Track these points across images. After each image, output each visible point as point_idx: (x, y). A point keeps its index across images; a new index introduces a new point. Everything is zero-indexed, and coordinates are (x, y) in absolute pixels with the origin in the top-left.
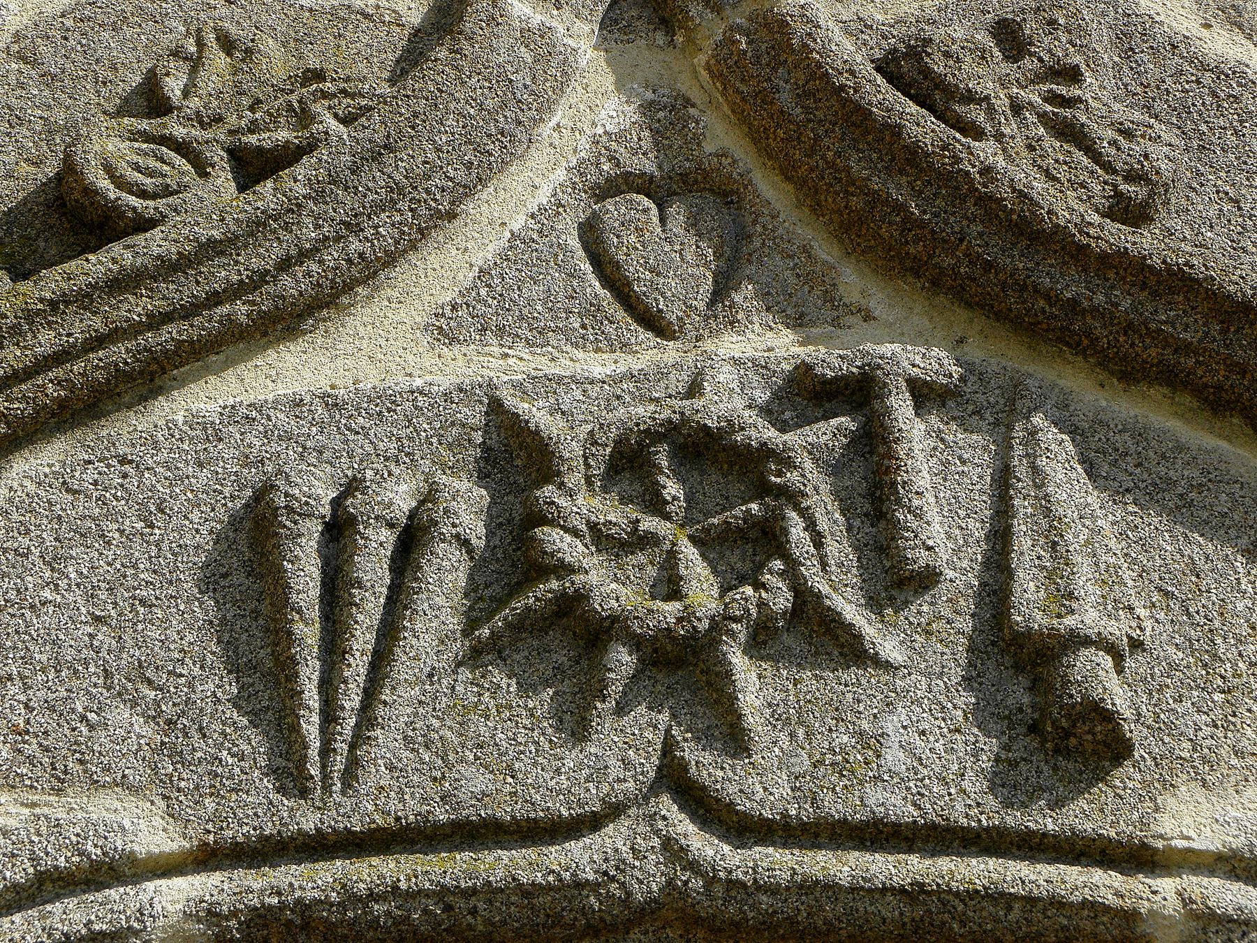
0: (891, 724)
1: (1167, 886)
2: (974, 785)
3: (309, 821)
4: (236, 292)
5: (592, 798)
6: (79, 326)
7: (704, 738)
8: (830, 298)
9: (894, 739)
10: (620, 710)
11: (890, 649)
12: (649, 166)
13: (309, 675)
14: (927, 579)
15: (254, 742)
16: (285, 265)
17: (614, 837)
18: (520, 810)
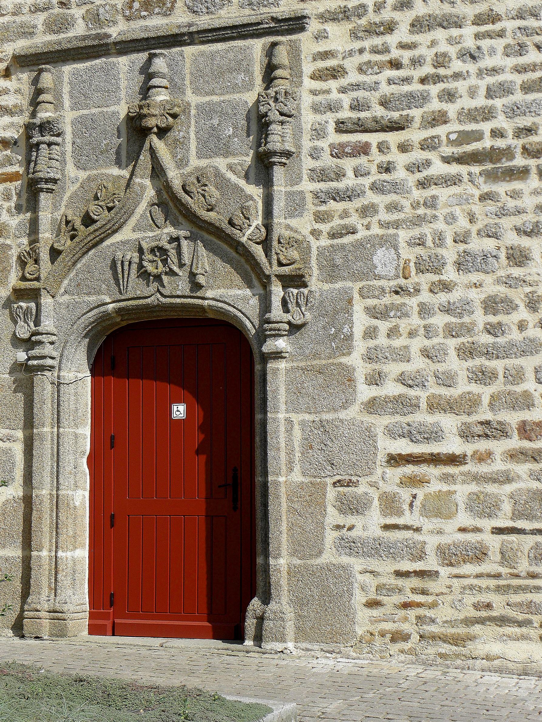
0: (180, 283)
1: (207, 301)
2: (188, 290)
3: (123, 298)
4: (109, 229)
5: (150, 294)
6: (92, 236)
7: (161, 286)
8: (178, 222)
9: (180, 285)
10: (152, 283)
11: (181, 274)
12: (157, 202)
13: (121, 283)
14: (185, 265)
15: (117, 288)
17: (152, 298)
18: (143, 296)
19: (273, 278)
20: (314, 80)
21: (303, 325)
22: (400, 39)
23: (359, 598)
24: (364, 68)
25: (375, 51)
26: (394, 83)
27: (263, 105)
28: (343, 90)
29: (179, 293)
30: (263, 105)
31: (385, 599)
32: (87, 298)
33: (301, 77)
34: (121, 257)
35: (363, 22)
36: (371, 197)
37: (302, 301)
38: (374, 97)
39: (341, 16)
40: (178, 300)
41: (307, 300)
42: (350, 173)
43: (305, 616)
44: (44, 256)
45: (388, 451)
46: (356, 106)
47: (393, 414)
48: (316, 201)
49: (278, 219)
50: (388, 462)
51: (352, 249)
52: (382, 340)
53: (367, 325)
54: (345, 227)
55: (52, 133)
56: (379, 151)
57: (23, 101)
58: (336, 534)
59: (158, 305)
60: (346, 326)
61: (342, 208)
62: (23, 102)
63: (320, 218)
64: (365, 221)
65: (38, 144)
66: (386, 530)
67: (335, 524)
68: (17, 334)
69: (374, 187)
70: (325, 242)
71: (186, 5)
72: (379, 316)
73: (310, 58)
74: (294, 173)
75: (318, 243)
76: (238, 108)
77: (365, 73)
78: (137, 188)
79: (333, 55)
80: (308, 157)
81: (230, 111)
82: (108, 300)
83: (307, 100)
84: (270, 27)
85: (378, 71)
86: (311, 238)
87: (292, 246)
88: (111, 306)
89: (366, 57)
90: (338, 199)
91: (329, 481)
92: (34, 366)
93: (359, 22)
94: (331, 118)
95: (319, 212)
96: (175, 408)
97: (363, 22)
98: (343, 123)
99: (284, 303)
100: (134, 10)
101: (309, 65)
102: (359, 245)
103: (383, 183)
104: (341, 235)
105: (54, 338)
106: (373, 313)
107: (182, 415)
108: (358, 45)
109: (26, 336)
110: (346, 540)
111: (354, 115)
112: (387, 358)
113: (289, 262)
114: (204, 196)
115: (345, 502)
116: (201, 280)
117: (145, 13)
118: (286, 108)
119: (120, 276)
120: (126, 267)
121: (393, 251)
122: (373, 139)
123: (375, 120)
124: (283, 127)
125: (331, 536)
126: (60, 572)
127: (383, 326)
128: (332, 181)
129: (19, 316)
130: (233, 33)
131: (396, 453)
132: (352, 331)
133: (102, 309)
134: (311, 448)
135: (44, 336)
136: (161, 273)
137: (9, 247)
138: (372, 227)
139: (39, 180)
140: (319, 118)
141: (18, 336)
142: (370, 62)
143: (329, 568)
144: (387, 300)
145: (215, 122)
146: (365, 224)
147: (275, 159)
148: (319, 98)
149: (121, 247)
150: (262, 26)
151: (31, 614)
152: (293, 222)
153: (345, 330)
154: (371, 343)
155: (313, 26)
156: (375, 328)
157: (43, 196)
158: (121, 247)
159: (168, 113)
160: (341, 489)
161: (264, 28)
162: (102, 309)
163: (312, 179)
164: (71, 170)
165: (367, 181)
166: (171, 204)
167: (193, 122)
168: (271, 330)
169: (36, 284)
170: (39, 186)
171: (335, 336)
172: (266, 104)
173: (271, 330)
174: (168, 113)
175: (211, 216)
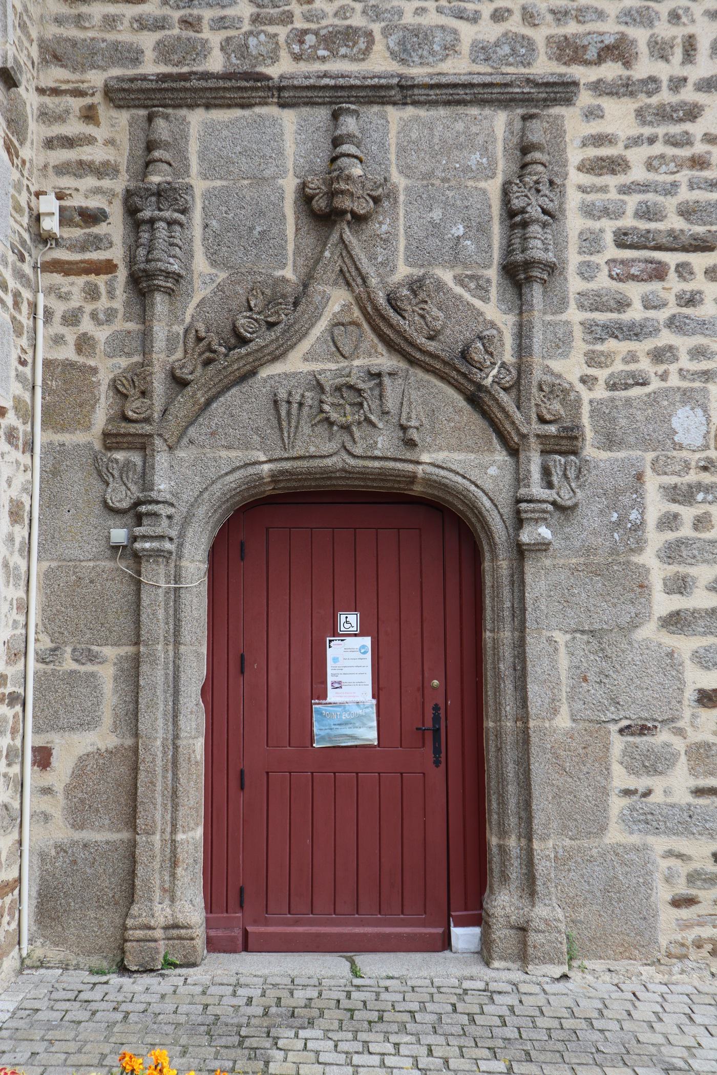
3: (286, 455)
4: (269, 354)
8: (376, 352)
11: (380, 425)
16: (277, 349)
17: (334, 459)
19: (533, 440)
21: (576, 505)
22: (705, 130)
23: (663, 894)
24: (655, 163)
25: (672, 142)
26: (700, 188)
27: (517, 198)
28: (625, 190)
29: (377, 453)
30: (517, 198)
31: (701, 894)
32: (224, 453)
33: (565, 166)
34: (285, 396)
35: (654, 100)
36: (666, 338)
37: (572, 474)
38: (670, 204)
39: (622, 90)
40: (377, 464)
41: (580, 472)
42: (637, 304)
43: (581, 922)
44: (159, 385)
45: (699, 686)
46: (647, 213)
47: (704, 634)
48: (588, 337)
49: (537, 360)
50: (699, 701)
51: (642, 405)
52: (686, 531)
53: (664, 510)
54: (632, 375)
55: (176, 207)
56: (679, 277)
57: (120, 156)
58: (626, 801)
59: (343, 470)
60: (634, 511)
61: (626, 350)
62: (119, 160)
63: (592, 360)
64: (661, 368)
65: (152, 221)
66: (699, 796)
67: (623, 787)
68: (109, 501)
69: (672, 323)
70: (601, 393)
71: (388, 48)
72: (680, 498)
73: (578, 142)
74: (556, 295)
75: (592, 395)
77: (656, 170)
78: (317, 298)
79: (610, 142)
81: (459, 203)
82: (263, 458)
83: (573, 199)
84: (523, 93)
85: (675, 170)
86: (580, 387)
87: (557, 396)
88: (266, 467)
89: (659, 148)
90: (620, 336)
91: (614, 728)
92: (144, 550)
93: (649, 101)
94: (608, 226)
95: (593, 352)
96: (343, 618)
97: (654, 100)
98: (625, 234)
99: (546, 472)
100: (307, 47)
101: (576, 151)
102: (653, 399)
103: (685, 320)
104: (627, 387)
105: (171, 511)
106: (675, 494)
107: (342, 629)
108: (647, 131)
109: (125, 505)
110: (641, 811)
111: (643, 225)
112: (694, 557)
113: (552, 418)
114: (423, 317)
115: (638, 757)
116: (414, 435)
117: (321, 53)
118: (552, 204)
119: (284, 424)
120: (294, 410)
121: (699, 411)
122: (671, 259)
123: (671, 233)
125: (617, 804)
126: (180, 864)
127: (688, 513)
128: (611, 311)
129: (111, 474)
130: (466, 94)
131: (710, 688)
132: (643, 518)
133: (251, 470)
134: (585, 680)
135: (161, 506)
136: (351, 424)
137: (94, 371)
138: (670, 378)
139: (158, 273)
140: (591, 224)
141: (111, 504)
142: (662, 156)
143: (616, 850)
144: (693, 477)
145: (437, 214)
146: (660, 373)
147: (536, 273)
148: (590, 198)
149: (285, 382)
150: (510, 90)
151: (139, 934)
152: (556, 365)
153: (632, 517)
154: (670, 536)
155: (585, 98)
156: (676, 516)
157: (159, 298)
158: (285, 382)
159: (368, 195)
160: (631, 739)
162: (251, 470)
163: (581, 307)
164: (200, 263)
165: (662, 315)
166: (365, 326)
167: (402, 213)
168: (533, 511)
169: (148, 429)
170: (156, 282)
171: (618, 524)
173: (533, 511)
174: (368, 195)
175: (431, 346)
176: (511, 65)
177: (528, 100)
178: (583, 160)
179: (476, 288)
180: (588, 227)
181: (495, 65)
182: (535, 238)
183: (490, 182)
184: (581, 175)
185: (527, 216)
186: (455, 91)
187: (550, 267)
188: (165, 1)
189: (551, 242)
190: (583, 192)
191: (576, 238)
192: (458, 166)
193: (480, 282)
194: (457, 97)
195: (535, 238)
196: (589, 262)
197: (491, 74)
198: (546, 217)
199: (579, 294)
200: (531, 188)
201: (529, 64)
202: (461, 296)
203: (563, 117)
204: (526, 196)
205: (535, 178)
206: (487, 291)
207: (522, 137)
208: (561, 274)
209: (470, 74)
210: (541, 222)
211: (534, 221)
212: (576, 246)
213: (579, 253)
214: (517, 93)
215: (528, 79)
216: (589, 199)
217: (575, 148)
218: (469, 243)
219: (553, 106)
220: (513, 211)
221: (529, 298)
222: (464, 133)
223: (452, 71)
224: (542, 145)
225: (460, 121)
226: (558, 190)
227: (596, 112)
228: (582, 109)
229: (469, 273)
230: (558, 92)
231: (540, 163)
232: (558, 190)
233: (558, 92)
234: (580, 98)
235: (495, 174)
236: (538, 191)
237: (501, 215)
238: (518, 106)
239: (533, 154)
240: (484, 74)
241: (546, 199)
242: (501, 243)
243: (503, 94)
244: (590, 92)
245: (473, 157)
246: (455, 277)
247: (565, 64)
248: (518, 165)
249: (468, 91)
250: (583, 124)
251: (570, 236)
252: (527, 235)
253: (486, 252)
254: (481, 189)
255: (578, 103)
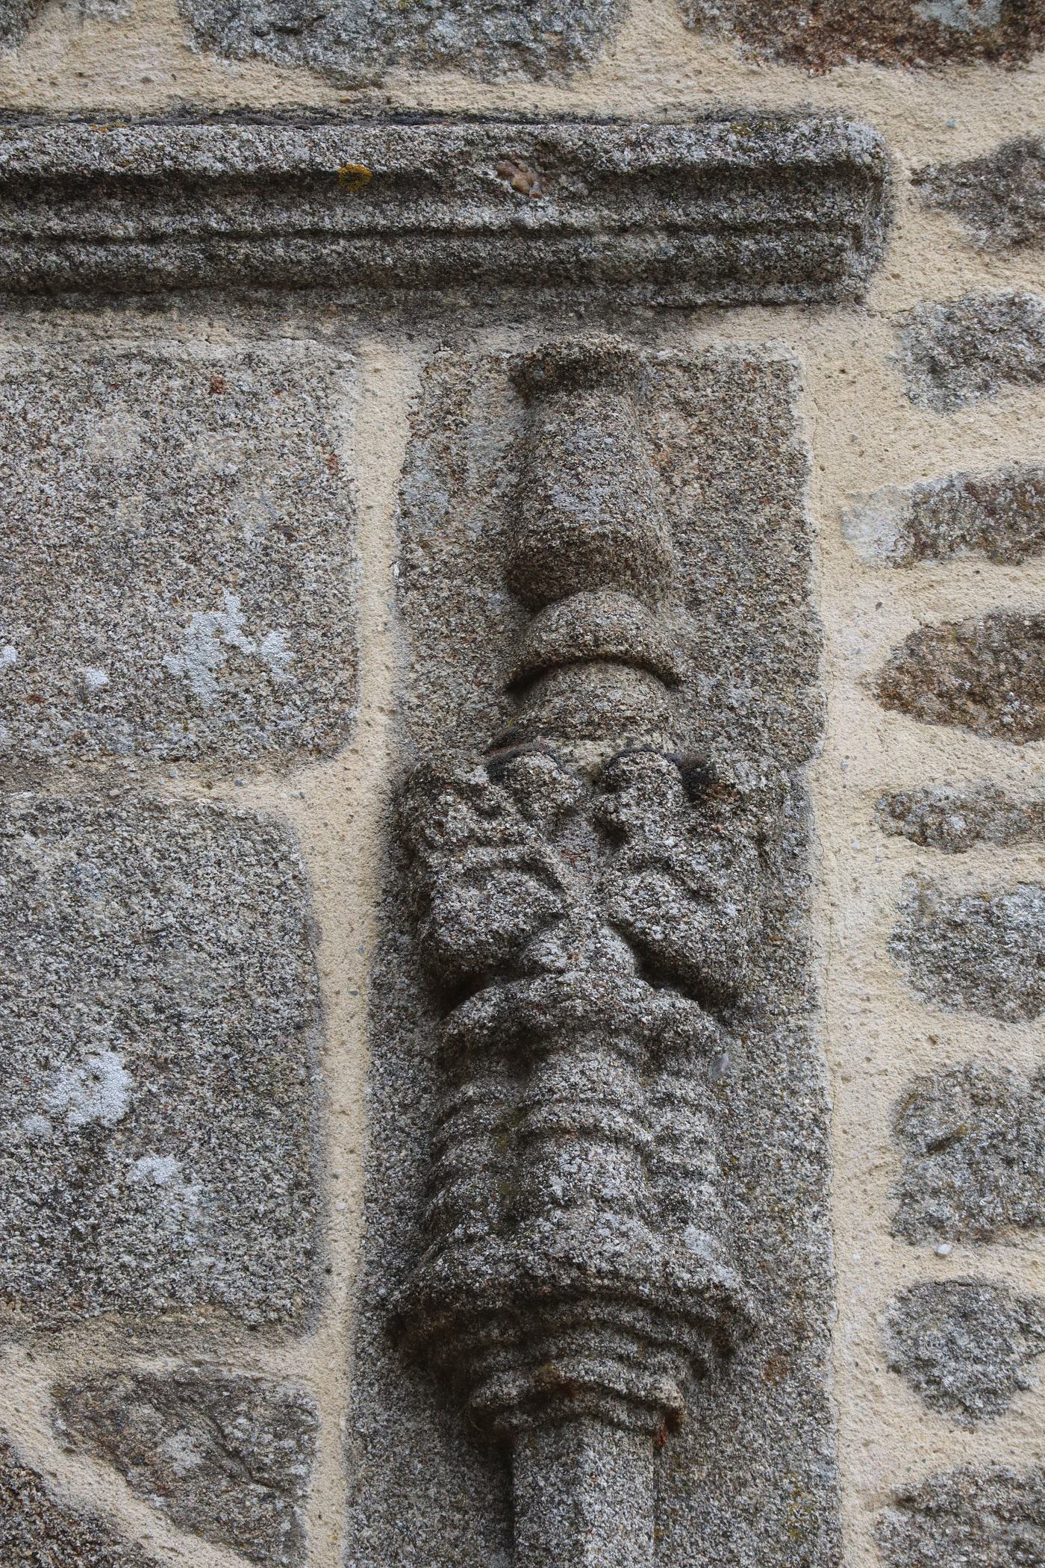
20: (920, 715)
27: (475, 876)
30: (475, 876)
76: (187, 890)
80: (880, 1380)
81: (101, 910)
84: (518, 229)
101: (872, 587)
118: (701, 918)
124: (667, 1083)
130: (154, 239)
150: (441, 214)
161: (448, 232)
172: (507, 865)
176: (448, 60)
177: (555, 275)
178: (915, 639)
179: (209, 1469)
180: (958, 1058)
181: (345, 63)
182: (589, 1132)
183: (309, 777)
184: (906, 731)
185: (534, 991)
186: (85, 222)
187: (698, 1323)
188: (101, 1)
189: (708, 1162)
190: (922, 838)
191: (883, 1131)
192: (98, 677)
193: (238, 1429)
194: (93, 256)
195: (589, 1132)
196: (969, 1287)
197: (323, 116)
198: (665, 1002)
199: (905, 1502)
200: (564, 815)
201: (565, 56)
202: (101, 1527)
203: (782, 373)
204: (533, 866)
205: (590, 753)
206: (283, 1488)
207: (515, 499)
208: (782, 1365)
209: (186, 114)
210: (633, 1028)
211: (582, 1026)
212: (882, 1184)
213: (904, 1231)
214: (483, 232)
215: (549, 147)
216: (959, 886)
217: (867, 567)
218: (164, 1167)
219: (719, 308)
220: (452, 959)
221: (556, 1529)
222: (140, 473)
223: (70, 98)
224: (645, 547)
225: (117, 402)
226: (745, 827)
227: (997, 346)
228: (905, 323)
229: (160, 1365)
230: (747, 229)
231: (624, 660)
232: (745, 827)
233: (747, 229)
234: (894, 262)
235: (340, 727)
236: (613, 834)
237: (380, 986)
238: (492, 315)
239: (580, 601)
240: (279, 117)
241: (661, 882)
242: (378, 1169)
243: (388, 235)
244: (956, 226)
245: (200, 621)
246: (64, 1398)
247: (794, 53)
248: (496, 674)
249: (161, 222)
250: (913, 417)
251: (836, 1122)
252: (538, 1118)
253: (281, 1229)
254: (247, 822)
255: (879, 293)
